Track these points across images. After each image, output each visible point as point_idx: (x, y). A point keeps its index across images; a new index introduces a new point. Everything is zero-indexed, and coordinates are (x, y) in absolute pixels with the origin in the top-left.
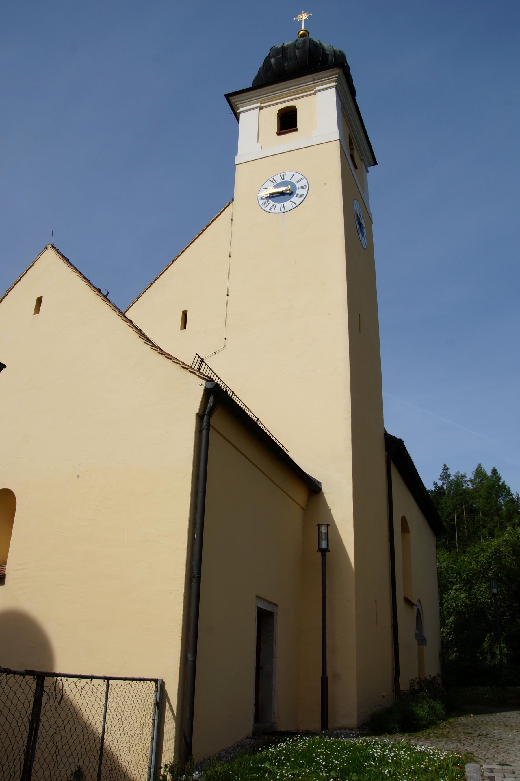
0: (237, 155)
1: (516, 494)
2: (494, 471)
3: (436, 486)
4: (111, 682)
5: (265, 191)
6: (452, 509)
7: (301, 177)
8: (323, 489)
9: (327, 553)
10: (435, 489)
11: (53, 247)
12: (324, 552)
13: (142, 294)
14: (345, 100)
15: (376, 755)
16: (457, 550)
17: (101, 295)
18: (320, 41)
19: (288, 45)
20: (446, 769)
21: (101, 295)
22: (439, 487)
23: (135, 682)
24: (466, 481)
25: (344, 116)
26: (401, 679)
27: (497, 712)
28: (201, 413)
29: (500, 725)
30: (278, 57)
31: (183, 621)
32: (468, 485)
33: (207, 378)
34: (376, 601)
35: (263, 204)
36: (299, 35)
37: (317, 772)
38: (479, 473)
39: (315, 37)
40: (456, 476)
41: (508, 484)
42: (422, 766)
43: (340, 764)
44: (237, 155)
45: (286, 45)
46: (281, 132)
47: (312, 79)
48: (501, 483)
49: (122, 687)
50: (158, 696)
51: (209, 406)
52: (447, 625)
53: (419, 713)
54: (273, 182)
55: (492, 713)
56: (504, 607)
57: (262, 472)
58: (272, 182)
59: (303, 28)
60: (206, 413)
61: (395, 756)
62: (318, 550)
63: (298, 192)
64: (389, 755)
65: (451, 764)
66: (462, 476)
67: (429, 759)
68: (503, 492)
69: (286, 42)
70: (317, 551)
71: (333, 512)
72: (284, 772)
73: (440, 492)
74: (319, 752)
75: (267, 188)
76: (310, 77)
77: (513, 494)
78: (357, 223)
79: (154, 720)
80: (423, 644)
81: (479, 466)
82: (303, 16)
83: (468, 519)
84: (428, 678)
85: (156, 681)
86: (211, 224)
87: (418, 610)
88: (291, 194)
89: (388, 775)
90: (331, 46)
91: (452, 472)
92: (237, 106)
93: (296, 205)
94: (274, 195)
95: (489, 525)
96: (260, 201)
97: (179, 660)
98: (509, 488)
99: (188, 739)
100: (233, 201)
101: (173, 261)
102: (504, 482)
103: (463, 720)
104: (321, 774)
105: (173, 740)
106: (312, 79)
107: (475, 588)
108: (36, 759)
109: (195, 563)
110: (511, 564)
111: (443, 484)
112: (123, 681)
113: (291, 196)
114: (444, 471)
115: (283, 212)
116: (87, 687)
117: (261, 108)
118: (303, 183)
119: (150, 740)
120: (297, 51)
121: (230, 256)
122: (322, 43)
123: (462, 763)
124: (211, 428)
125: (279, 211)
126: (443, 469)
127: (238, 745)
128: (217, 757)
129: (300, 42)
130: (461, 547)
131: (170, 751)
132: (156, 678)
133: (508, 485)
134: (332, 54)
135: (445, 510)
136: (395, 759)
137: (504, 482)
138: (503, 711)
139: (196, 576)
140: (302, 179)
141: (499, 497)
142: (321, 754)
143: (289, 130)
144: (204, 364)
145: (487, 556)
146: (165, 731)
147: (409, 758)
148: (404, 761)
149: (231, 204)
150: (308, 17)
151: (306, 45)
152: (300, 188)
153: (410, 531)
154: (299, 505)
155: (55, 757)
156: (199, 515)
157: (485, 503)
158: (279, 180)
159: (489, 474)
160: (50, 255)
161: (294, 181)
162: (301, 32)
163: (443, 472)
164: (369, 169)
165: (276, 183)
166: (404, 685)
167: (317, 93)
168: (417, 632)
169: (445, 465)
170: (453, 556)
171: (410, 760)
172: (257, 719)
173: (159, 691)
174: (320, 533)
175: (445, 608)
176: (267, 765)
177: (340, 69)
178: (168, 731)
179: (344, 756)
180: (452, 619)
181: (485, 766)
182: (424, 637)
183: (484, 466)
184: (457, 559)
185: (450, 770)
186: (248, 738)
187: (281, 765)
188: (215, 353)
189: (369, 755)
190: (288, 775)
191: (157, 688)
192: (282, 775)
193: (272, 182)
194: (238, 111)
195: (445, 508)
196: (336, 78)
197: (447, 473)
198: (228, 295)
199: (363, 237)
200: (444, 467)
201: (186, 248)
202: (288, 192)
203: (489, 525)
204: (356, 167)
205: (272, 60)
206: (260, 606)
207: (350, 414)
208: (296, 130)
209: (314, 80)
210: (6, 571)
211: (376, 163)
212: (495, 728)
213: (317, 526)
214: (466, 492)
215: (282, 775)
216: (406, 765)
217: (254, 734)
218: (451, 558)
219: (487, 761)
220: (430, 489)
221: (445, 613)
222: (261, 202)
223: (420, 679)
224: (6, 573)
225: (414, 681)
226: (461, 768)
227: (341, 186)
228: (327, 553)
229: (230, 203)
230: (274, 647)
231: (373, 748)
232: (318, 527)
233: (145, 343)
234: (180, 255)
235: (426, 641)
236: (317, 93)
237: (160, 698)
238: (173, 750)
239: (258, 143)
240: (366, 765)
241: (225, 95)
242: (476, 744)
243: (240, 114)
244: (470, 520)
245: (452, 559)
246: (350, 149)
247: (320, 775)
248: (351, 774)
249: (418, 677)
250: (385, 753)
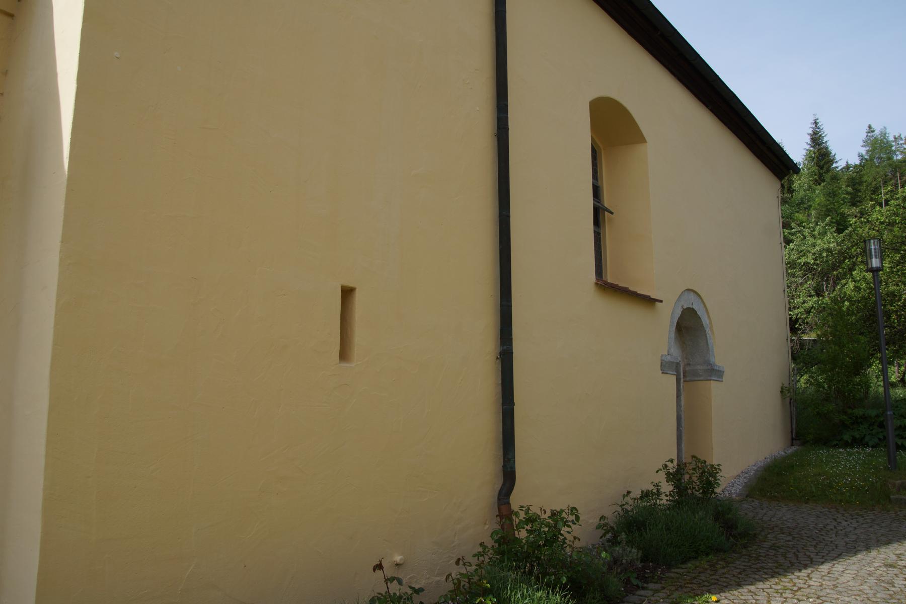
3: (862, 159)
24: (901, 144)
107: (855, 191)
114: (869, 134)
126: (866, 132)
128: (798, 364)
153: (647, 139)
163: (867, 135)
169: (870, 127)
197: (872, 136)
200: (868, 128)
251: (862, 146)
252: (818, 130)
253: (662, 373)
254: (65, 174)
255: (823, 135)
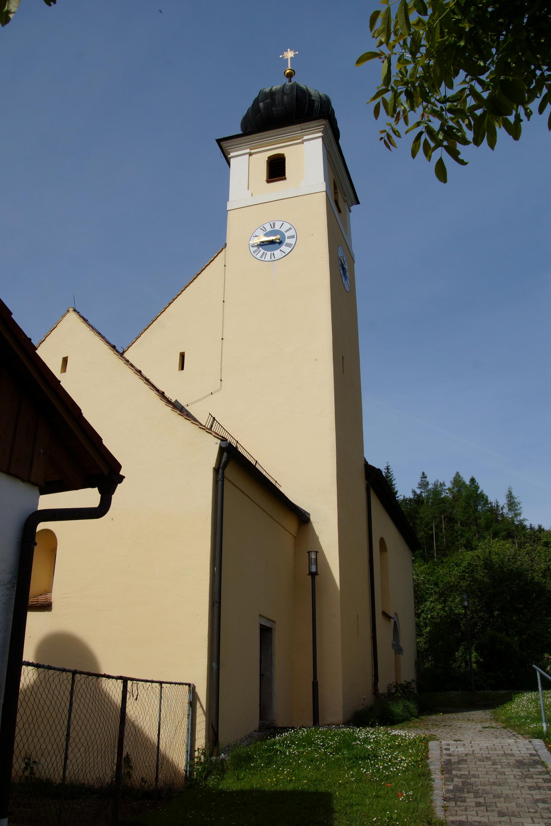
0: (228, 200)
1: (495, 502)
2: (473, 480)
4: (163, 685)
5: (256, 239)
6: (430, 518)
7: (290, 226)
8: (311, 520)
9: (316, 576)
10: (413, 497)
11: (75, 310)
12: (313, 575)
13: (141, 335)
14: (330, 148)
15: (361, 738)
16: (435, 559)
17: (123, 360)
18: (307, 86)
19: (276, 90)
20: (414, 745)
21: (123, 360)
22: (417, 494)
23: (177, 685)
24: (445, 489)
25: (330, 164)
26: (379, 685)
27: (464, 712)
28: (217, 467)
29: (463, 720)
30: (266, 101)
31: (208, 637)
32: (447, 493)
33: (221, 438)
34: (358, 616)
35: (254, 252)
36: (286, 74)
37: (316, 750)
38: (457, 481)
39: (301, 81)
40: (436, 485)
41: (486, 493)
42: (396, 743)
43: (334, 744)
44: (228, 201)
45: (274, 90)
46: (270, 180)
47: (300, 128)
48: (479, 492)
49: (170, 689)
50: (191, 696)
51: (223, 461)
52: (423, 636)
53: (395, 710)
54: (264, 231)
55: (460, 712)
56: (476, 618)
57: (262, 509)
58: (263, 230)
59: (290, 68)
60: (221, 467)
61: (376, 737)
62: (308, 573)
63: (287, 241)
64: (371, 737)
65: (418, 741)
66: (441, 484)
67: (402, 739)
68: (481, 501)
69: (275, 86)
70: (308, 575)
71: (321, 540)
72: (291, 750)
73: (418, 500)
74: (316, 737)
75: (258, 236)
76: (298, 127)
77: (492, 503)
78: (341, 268)
79: (189, 715)
80: (400, 654)
81: (458, 475)
82: (290, 54)
83: (447, 528)
84: (404, 683)
85: (189, 685)
86: (205, 269)
87: (395, 622)
88: (281, 243)
89: (371, 749)
90: (317, 91)
91: (431, 480)
92: (228, 150)
93: (284, 255)
94: (265, 243)
95: (467, 535)
96: (251, 248)
97: (207, 668)
98: (487, 497)
99: (216, 729)
100: (226, 247)
101: (170, 304)
102: (482, 491)
103: (434, 717)
104: (320, 751)
105: (204, 730)
106: (300, 128)
108: (125, 738)
109: (216, 591)
110: (483, 577)
111: (421, 492)
112: (169, 685)
113: (281, 245)
114: (423, 479)
115: (273, 261)
116: (150, 689)
117: (251, 154)
118: (292, 233)
119: (186, 730)
120: (285, 97)
121: (224, 301)
122: (308, 88)
123: (426, 741)
124: (225, 479)
125: (269, 260)
126: (421, 478)
127: (248, 736)
129: (288, 87)
130: (439, 557)
131: (202, 739)
132: (190, 683)
133: (486, 495)
134: (318, 100)
135: (423, 519)
136: (375, 739)
137: (482, 491)
138: (470, 711)
139: (217, 601)
140: (290, 229)
141: (477, 506)
142: (318, 738)
143: (278, 178)
144: (215, 421)
145: (461, 569)
146: (197, 724)
147: (386, 739)
148: (382, 741)
149: (224, 250)
150: (295, 55)
151: (294, 92)
152: (289, 237)
153: (388, 550)
154: (291, 533)
155: (135, 737)
156: (218, 551)
157: (463, 512)
158: (269, 229)
159: (468, 482)
160: (72, 317)
161: (283, 230)
162: (288, 71)
163: (421, 480)
164: (352, 208)
165: (266, 232)
166: (382, 688)
167: (304, 143)
168: (394, 642)
169: (423, 474)
170: (430, 567)
171: (387, 740)
172: (261, 718)
173: (191, 693)
174: (310, 559)
175: (422, 619)
176: (277, 747)
177: (326, 120)
178: (199, 723)
179: (336, 739)
180: (428, 629)
181: (444, 742)
182: (401, 647)
183: (462, 474)
184: (434, 569)
185: (417, 745)
186: (255, 731)
187: (289, 747)
188: (211, 393)
189: (355, 738)
190: (295, 753)
191: (190, 691)
192: (290, 753)
193: (263, 230)
194: (229, 156)
195: (423, 517)
196: (323, 129)
197: (425, 481)
198: (222, 339)
199: (346, 281)
201: (182, 292)
202: (278, 241)
203: (467, 535)
204: (340, 211)
205: (261, 104)
206: (262, 623)
207: (336, 452)
208: (285, 179)
209: (302, 129)
210: (52, 599)
211: (358, 203)
212: (459, 721)
213: (307, 552)
214: (444, 501)
215: (290, 753)
216: (384, 743)
217: (260, 729)
218: (429, 568)
219: (446, 739)
220: (408, 498)
221: (422, 624)
222: (253, 249)
223: (396, 683)
224: (52, 601)
225: (391, 685)
226: (425, 744)
227: (327, 237)
228: (316, 576)
229: (222, 249)
230: (273, 657)
231: (359, 733)
232: (308, 554)
233: (166, 405)
234: (176, 298)
235: (402, 650)
236: (304, 143)
237: (192, 698)
238: (204, 738)
239: (248, 189)
240: (354, 744)
241: (216, 140)
242: (440, 730)
243: (231, 159)
244: (449, 528)
245: (430, 570)
246: (334, 193)
247: (319, 752)
248: (343, 750)
249: (394, 682)
250: (368, 736)
251: (417, 488)
252: (389, 475)
253: (274, 622)
254: (441, 40)
255: (393, 479)
